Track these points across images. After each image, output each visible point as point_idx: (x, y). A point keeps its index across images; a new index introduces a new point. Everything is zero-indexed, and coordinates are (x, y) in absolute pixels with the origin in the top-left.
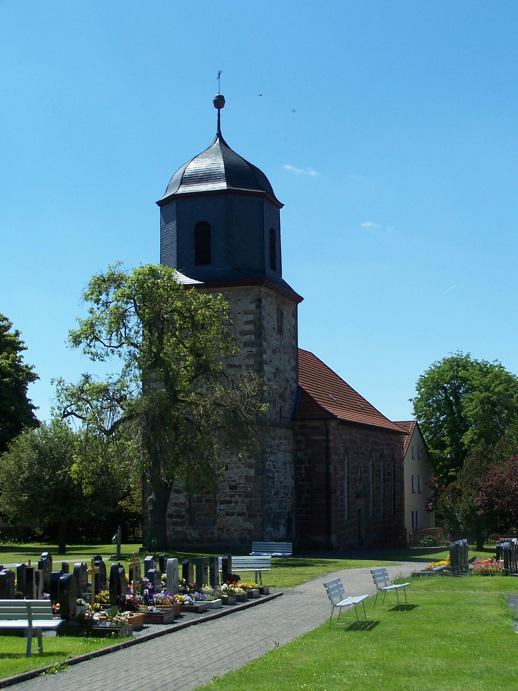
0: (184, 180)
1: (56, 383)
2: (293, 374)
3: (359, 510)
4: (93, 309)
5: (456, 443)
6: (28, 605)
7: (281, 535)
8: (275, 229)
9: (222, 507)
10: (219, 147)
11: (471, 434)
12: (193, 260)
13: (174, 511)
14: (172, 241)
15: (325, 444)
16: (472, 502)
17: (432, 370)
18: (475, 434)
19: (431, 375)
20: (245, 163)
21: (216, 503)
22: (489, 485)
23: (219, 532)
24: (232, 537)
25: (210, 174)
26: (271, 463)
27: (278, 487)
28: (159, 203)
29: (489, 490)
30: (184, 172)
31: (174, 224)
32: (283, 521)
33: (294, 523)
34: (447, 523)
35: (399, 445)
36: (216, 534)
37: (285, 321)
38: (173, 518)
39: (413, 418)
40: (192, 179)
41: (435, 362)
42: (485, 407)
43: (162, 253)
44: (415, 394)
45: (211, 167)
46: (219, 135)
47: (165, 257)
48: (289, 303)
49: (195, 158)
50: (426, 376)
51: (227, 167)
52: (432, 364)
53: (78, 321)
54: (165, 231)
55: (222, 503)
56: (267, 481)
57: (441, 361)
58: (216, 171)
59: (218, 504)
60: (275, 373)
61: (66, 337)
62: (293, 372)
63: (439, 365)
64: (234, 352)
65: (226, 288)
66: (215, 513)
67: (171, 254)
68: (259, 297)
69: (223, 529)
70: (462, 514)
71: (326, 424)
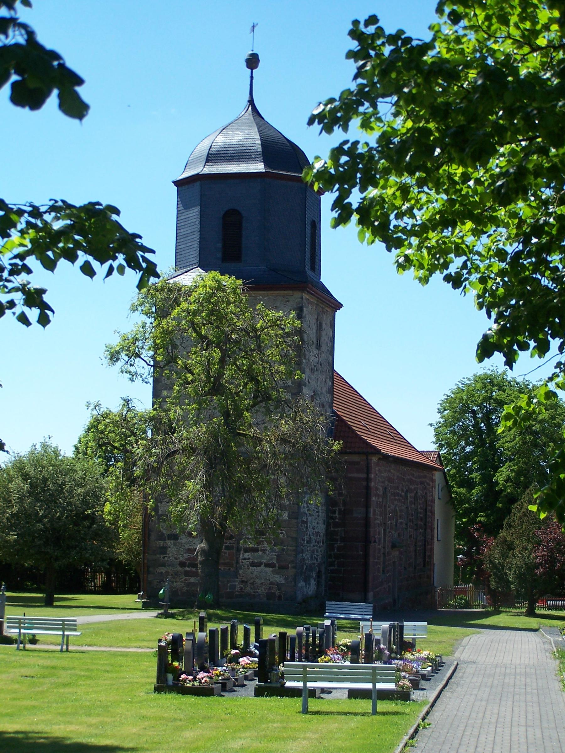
0: (211, 157)
1: (92, 406)
2: (328, 397)
3: (394, 562)
4: (146, 324)
5: (488, 480)
6: (305, 667)
7: (311, 592)
8: (316, 221)
9: (247, 555)
10: (252, 118)
11: (508, 471)
12: (219, 255)
13: (186, 559)
14: (193, 230)
15: (364, 483)
16: (528, 558)
17: (459, 388)
18: (512, 471)
19: (459, 395)
20: (285, 140)
21: (239, 550)
22: (551, 539)
23: (242, 586)
24: (257, 592)
25: (243, 151)
26: (305, 505)
27: (311, 534)
28: (177, 183)
29: (551, 544)
30: (211, 147)
31: (197, 210)
32: (314, 575)
33: (323, 577)
34: (495, 582)
35: (431, 483)
36: (238, 588)
37: (323, 333)
38: (185, 566)
39: (433, 447)
40: (221, 157)
41: (464, 378)
42: (525, 438)
43: (178, 244)
44: (437, 418)
45: (245, 143)
46: (251, 102)
47: (183, 249)
48: (327, 311)
49: (223, 129)
50: (453, 396)
51: (264, 144)
52: (459, 380)
53: (116, 333)
54: (183, 218)
55: (247, 550)
56: (301, 526)
57: (472, 378)
58: (251, 148)
59: (242, 552)
60: (312, 396)
61: (102, 353)
62: (328, 395)
63: (469, 382)
64: (298, 378)
65: (260, 292)
66: (237, 562)
67: (191, 247)
68: (301, 305)
69: (246, 582)
70: (515, 571)
71: (367, 458)
